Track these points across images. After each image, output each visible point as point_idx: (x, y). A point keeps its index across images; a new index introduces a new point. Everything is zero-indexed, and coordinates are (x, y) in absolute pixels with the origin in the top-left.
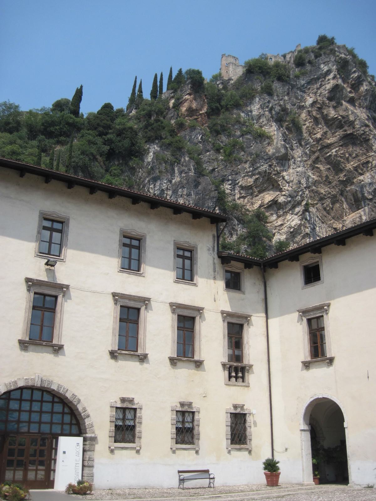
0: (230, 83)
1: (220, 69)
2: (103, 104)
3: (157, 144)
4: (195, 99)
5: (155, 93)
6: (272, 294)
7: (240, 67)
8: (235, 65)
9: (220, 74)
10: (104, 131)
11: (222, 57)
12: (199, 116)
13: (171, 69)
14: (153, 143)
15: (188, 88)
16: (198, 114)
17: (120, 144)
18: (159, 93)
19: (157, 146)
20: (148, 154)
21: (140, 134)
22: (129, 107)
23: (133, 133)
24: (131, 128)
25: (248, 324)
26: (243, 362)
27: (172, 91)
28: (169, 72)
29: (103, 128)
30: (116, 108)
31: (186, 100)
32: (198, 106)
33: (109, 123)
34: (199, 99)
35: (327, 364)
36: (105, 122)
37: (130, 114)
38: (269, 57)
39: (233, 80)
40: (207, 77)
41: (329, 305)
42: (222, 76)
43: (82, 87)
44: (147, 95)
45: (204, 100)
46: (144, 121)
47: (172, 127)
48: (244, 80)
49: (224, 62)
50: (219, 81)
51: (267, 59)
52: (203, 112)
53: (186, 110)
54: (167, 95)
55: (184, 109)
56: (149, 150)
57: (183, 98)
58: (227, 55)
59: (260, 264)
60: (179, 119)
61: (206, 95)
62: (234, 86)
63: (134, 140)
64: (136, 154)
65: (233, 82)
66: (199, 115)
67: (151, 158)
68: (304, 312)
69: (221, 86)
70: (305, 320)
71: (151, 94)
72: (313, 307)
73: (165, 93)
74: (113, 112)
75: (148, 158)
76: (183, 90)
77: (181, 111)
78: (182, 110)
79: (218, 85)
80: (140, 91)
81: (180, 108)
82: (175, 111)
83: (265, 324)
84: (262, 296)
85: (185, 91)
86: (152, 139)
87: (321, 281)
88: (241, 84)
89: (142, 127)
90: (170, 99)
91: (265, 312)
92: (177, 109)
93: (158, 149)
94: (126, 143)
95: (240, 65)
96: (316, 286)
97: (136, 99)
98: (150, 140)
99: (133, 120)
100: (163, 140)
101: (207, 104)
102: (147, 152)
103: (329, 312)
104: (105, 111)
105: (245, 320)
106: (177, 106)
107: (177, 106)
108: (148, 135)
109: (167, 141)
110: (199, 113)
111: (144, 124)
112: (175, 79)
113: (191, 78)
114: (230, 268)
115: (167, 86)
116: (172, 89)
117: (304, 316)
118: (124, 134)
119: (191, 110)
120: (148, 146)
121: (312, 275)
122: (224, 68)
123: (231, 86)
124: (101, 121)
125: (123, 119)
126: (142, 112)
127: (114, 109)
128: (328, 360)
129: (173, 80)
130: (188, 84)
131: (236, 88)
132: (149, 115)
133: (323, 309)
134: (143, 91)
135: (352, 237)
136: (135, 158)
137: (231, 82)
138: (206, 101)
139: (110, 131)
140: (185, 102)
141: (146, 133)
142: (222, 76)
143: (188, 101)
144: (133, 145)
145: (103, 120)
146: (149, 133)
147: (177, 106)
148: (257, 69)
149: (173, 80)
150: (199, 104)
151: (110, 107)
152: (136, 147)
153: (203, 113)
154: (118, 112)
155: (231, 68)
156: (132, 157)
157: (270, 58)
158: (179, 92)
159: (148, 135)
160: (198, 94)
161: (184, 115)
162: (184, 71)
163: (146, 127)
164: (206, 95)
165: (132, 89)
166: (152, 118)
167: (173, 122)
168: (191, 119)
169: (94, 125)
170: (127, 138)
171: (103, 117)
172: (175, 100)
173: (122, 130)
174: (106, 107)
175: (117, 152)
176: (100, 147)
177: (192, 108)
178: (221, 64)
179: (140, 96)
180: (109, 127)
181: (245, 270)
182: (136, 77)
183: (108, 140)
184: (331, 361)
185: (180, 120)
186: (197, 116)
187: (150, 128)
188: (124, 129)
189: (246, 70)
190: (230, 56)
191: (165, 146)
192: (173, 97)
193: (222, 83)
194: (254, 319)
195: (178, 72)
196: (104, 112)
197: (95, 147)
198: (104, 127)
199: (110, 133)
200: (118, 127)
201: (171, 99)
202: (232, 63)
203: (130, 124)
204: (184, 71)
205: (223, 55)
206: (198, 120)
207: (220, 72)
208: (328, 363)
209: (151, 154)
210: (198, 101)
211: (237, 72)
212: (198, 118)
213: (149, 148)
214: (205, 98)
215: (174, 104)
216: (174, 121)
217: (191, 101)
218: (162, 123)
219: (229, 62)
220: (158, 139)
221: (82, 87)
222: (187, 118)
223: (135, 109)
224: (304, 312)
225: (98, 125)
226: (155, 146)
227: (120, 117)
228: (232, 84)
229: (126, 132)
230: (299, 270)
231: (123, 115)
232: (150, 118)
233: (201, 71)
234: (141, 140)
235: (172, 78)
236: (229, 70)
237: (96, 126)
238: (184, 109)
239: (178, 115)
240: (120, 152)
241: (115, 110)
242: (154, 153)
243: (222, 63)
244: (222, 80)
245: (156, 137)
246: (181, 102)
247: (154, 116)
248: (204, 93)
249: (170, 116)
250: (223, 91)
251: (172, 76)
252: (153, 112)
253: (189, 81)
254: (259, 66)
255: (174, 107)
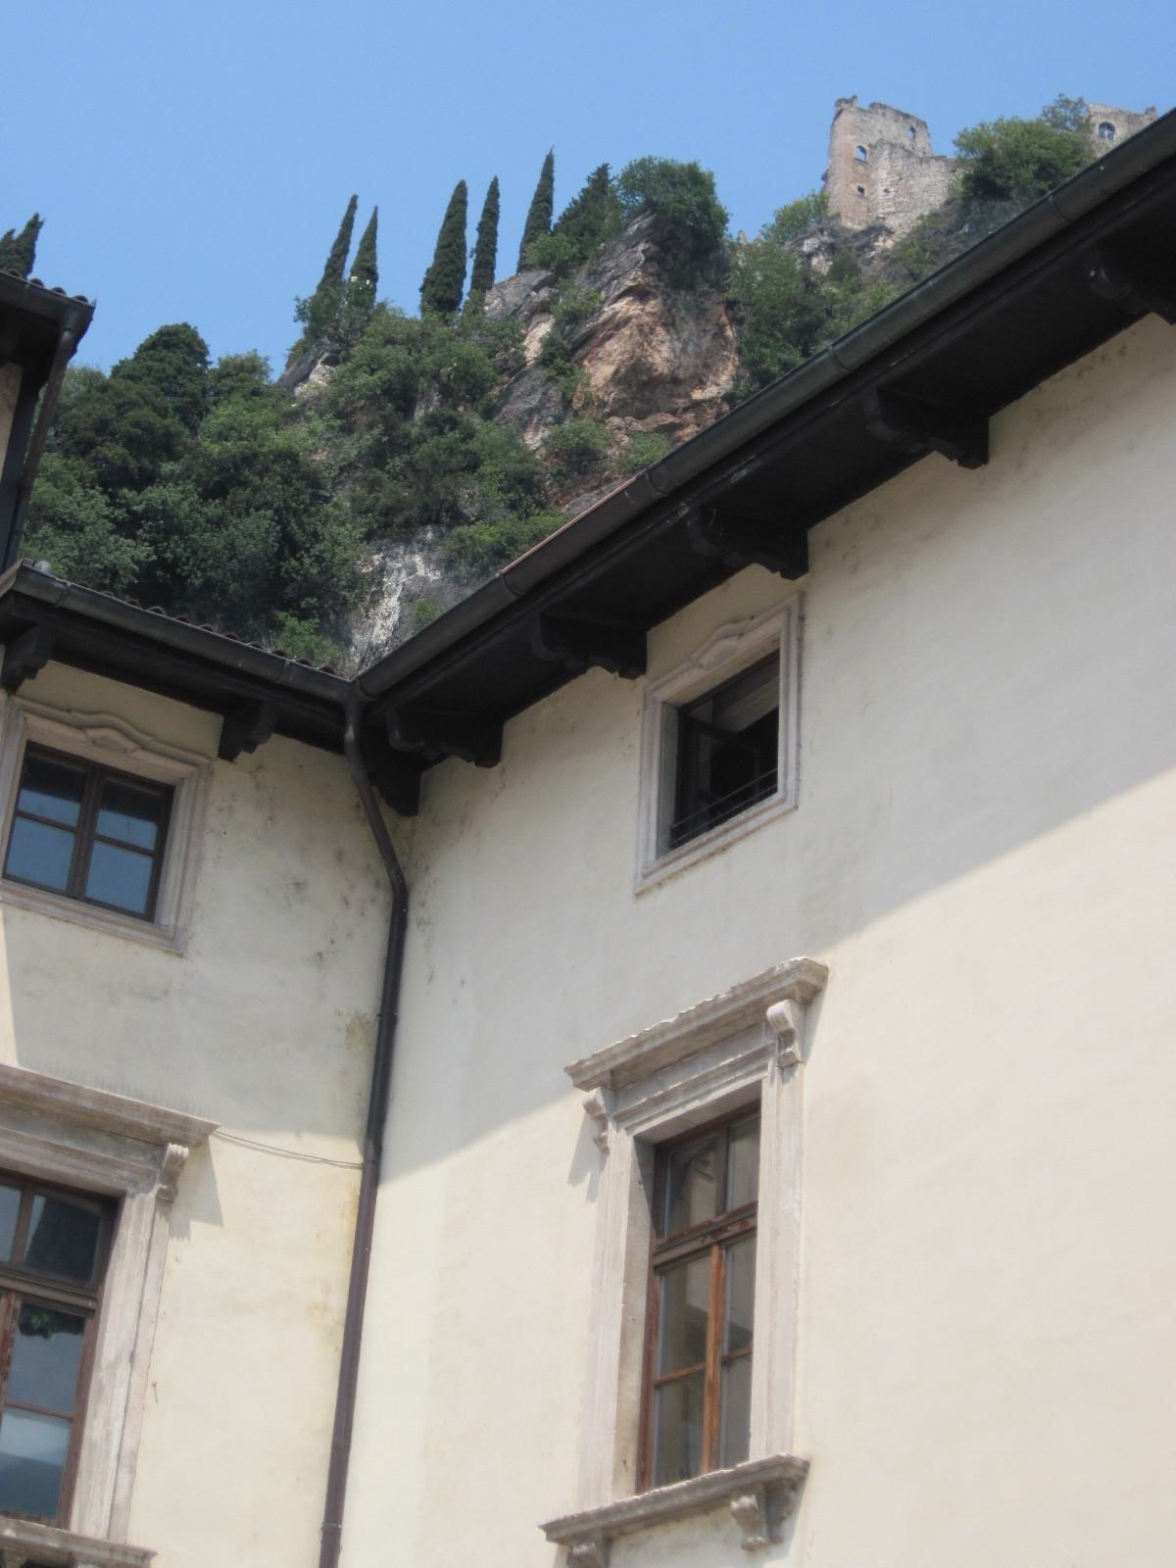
0: (872, 248)
1: (825, 178)
2: (154, 330)
3: (429, 547)
4: (669, 323)
5: (448, 285)
6: (430, 979)
7: (934, 166)
8: (909, 154)
9: (821, 203)
10: (133, 464)
11: (839, 113)
12: (689, 416)
13: (549, 162)
14: (408, 542)
15: (630, 262)
16: (681, 403)
17: (217, 541)
18: (475, 284)
19: (427, 561)
20: (375, 603)
21: (342, 497)
22: (301, 359)
23: (298, 484)
24: (288, 456)
25: (166, 1200)
26: (65, 1522)
27: (544, 274)
28: (535, 178)
29: (125, 445)
30: (220, 348)
31: (617, 324)
32: (685, 360)
33: (173, 423)
34: (691, 324)
35: (739, 1535)
36: (145, 414)
37: (298, 390)
38: (1098, 120)
39: (890, 232)
40: (747, 219)
41: (808, 993)
42: (832, 211)
43: (34, 225)
44: (401, 289)
45: (721, 329)
46: (370, 427)
47: (520, 461)
48: (950, 232)
49: (848, 140)
50: (812, 235)
51: (1084, 126)
52: (711, 391)
53: (616, 379)
54: (512, 296)
55: (600, 372)
56: (380, 584)
57: (600, 311)
58: (863, 103)
59: (336, 708)
60: (567, 424)
61: (730, 305)
62: (894, 261)
63: (301, 525)
64: (303, 604)
65: (889, 243)
66: (686, 410)
67: (390, 623)
68: (620, 1080)
69: (821, 264)
70: (622, 1144)
71: (422, 289)
72: (684, 1019)
73: (502, 286)
74: (200, 373)
75: (372, 626)
76: (605, 271)
77: (588, 385)
78: (589, 377)
79: (809, 256)
80: (368, 270)
81: (581, 366)
82: (550, 379)
83: (345, 1226)
84: (364, 1000)
85: (614, 278)
86: (399, 519)
87: (775, 797)
88: (934, 252)
89: (360, 457)
90: (528, 320)
91: (359, 1124)
92: (562, 372)
93: (434, 576)
94: (252, 533)
95: (938, 153)
96: (738, 850)
97: (339, 308)
98: (392, 527)
99: (308, 419)
100: (464, 530)
101: (739, 351)
102: (370, 589)
103: (805, 1053)
104: (156, 365)
105: (138, 1161)
106: (568, 355)
107: (564, 356)
108: (383, 501)
109: (485, 535)
110: (688, 396)
111: (368, 439)
112: (565, 218)
113: (650, 206)
114: (82, 727)
115: (522, 251)
116: (544, 265)
117: (619, 1119)
118: (244, 484)
119: (644, 378)
120: (377, 558)
121: (722, 768)
122: (843, 169)
123: (878, 264)
124: (121, 409)
125: (250, 410)
126: (363, 379)
127: (208, 359)
128: (745, 1490)
129: (555, 219)
130: (631, 244)
131: (905, 271)
132: (401, 395)
133: (760, 1022)
134: (382, 266)
135: (1046, 385)
136: (292, 622)
137: (879, 244)
138: (730, 333)
139: (167, 467)
140: (610, 337)
141: (374, 485)
142: (832, 211)
143: (626, 331)
144: (289, 545)
145: (133, 404)
146: (390, 485)
147: (564, 356)
148: (1027, 173)
149: (555, 219)
150: (690, 348)
151: (189, 345)
152: (307, 561)
153: (711, 401)
154: (229, 375)
155: (883, 173)
156: (282, 615)
157: (1104, 126)
158: (580, 278)
159: (383, 501)
160: (685, 297)
161: (604, 404)
162: (616, 172)
163: (378, 456)
164: (730, 305)
165: (324, 262)
166: (419, 413)
167: (533, 440)
168: (638, 426)
169: (75, 430)
170: (257, 509)
171: (133, 391)
172: (556, 325)
173: (236, 468)
174: (167, 346)
175: (197, 582)
176: (93, 547)
177: (650, 368)
178: (831, 153)
179: (364, 296)
180: (166, 447)
181: (221, 765)
182: (354, 199)
183: (149, 513)
184: (777, 1492)
185: (577, 433)
186: (674, 413)
187: (397, 462)
188: (249, 460)
189: (967, 178)
190: (884, 107)
191: (475, 559)
192: (544, 309)
193: (832, 249)
194: (235, 1165)
195: (586, 185)
196: (150, 369)
197: (63, 542)
198: (131, 442)
199: (173, 478)
200: (216, 449)
201: (536, 318)
202: (893, 146)
203: (296, 436)
204: (616, 172)
205: (843, 104)
206: (680, 433)
207: (824, 189)
208: (745, 1518)
209: (392, 603)
210: (685, 335)
211: (915, 189)
212: (681, 426)
213: (382, 570)
214: (724, 319)
215: (548, 343)
216: (544, 433)
217: (645, 333)
218: (469, 435)
219: (873, 141)
220: (438, 522)
221: (34, 225)
222: (616, 420)
223: (332, 361)
224: (620, 1080)
225: (102, 427)
226: (418, 559)
227: (236, 397)
228: (885, 256)
229: (257, 480)
230: (637, 742)
231: (255, 393)
232: (407, 411)
233: (711, 175)
234: (343, 524)
235: (548, 211)
236: (873, 184)
237: (91, 435)
238: (600, 372)
239: (567, 403)
240: (209, 585)
241: (215, 366)
242: (408, 598)
243: (838, 143)
244: (832, 234)
245: (425, 508)
246: (590, 335)
247: (429, 401)
248: (722, 290)
249: (522, 406)
250: (830, 289)
251: (549, 201)
252: (423, 383)
253: (642, 222)
254: (1039, 160)
255: (545, 361)
